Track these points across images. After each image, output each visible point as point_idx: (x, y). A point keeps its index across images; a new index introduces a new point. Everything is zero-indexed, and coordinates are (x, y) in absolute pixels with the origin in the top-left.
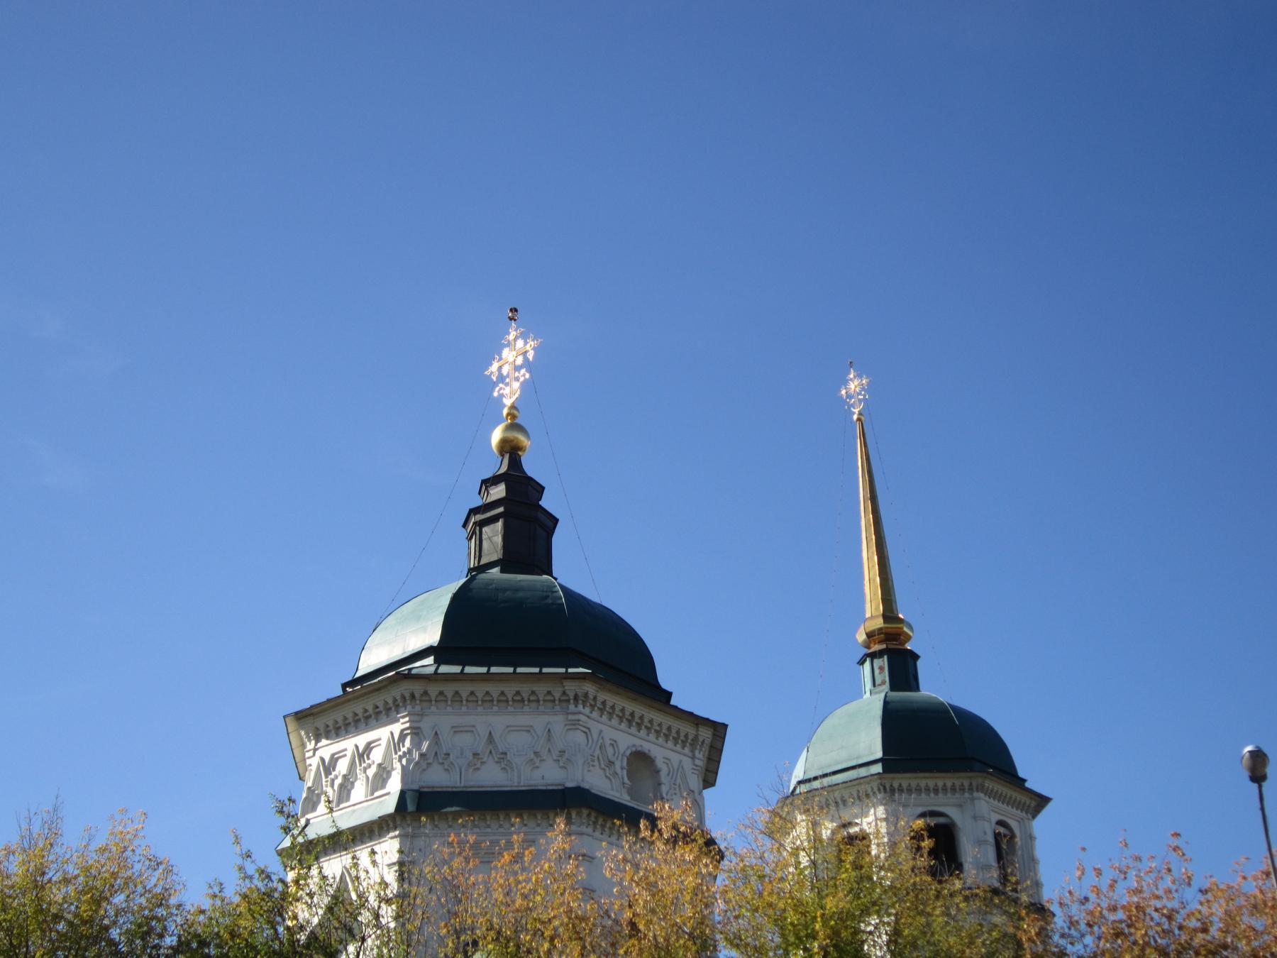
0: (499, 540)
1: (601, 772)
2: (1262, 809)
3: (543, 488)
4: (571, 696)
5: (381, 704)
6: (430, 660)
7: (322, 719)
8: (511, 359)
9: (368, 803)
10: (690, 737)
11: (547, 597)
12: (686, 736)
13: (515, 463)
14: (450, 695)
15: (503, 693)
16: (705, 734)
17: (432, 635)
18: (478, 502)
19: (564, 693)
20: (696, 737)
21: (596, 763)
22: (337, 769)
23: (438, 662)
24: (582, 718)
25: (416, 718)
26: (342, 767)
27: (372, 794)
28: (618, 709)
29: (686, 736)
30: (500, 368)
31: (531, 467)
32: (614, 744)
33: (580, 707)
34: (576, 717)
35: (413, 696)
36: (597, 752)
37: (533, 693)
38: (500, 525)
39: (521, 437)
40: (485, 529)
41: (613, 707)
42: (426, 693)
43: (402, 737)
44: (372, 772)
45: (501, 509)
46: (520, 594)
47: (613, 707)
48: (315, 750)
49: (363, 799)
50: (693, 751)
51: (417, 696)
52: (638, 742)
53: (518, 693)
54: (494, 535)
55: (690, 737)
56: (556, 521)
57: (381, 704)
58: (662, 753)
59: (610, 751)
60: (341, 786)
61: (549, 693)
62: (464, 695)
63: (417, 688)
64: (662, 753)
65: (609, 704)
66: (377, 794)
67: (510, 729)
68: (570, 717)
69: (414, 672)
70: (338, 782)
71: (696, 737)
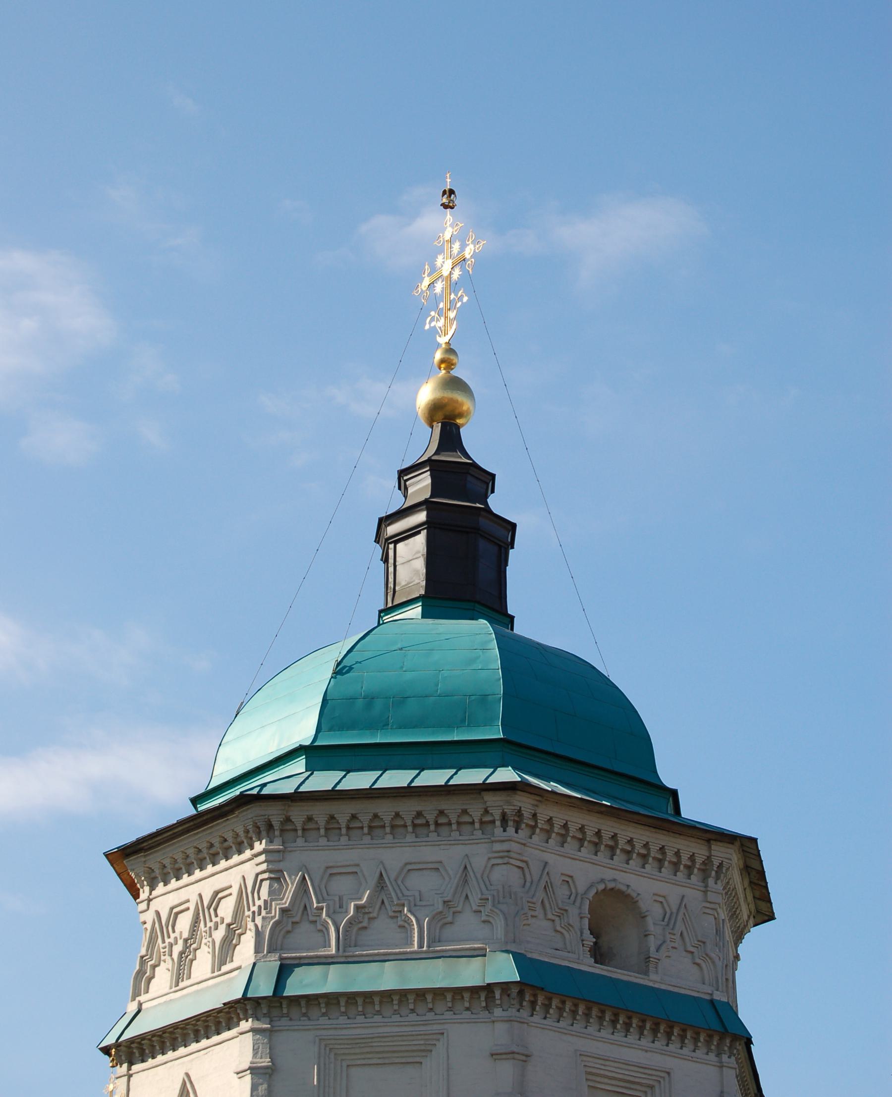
0: (420, 565)
1: (548, 924)
2: (233, 1038)
3: (493, 476)
4: (497, 814)
5: (229, 836)
6: (299, 765)
7: (143, 859)
8: (446, 272)
9: (212, 985)
10: (699, 860)
11: (473, 660)
12: (692, 858)
13: (450, 437)
14: (322, 821)
15: (397, 815)
16: (731, 856)
17: (303, 729)
18: (397, 502)
19: (486, 811)
20: (708, 861)
21: (539, 912)
22: (178, 928)
23: (311, 768)
24: (514, 847)
25: (276, 856)
26: (227, 909)
27: (177, 985)
28: (573, 829)
29: (692, 858)
30: (431, 285)
31: (479, 445)
32: (569, 880)
33: (511, 830)
34: (505, 846)
35: (270, 827)
36: (541, 895)
37: (441, 813)
38: (420, 540)
39: (459, 397)
40: (400, 546)
41: (565, 826)
42: (288, 820)
43: (257, 883)
44: (219, 935)
45: (421, 517)
46: (409, 676)
47: (565, 826)
48: (149, 900)
49: (167, 990)
50: (704, 880)
51: (276, 825)
52: (609, 874)
53: (419, 814)
54: (412, 557)
55: (699, 860)
56: (513, 526)
57: (229, 836)
58: (647, 885)
59: (562, 892)
60: (181, 953)
61: (465, 812)
62: (343, 820)
63: (275, 813)
64: (647, 885)
65: (558, 823)
66: (225, 969)
67: (409, 869)
68: (497, 847)
69: (265, 791)
70: (177, 949)
71: (708, 861)
